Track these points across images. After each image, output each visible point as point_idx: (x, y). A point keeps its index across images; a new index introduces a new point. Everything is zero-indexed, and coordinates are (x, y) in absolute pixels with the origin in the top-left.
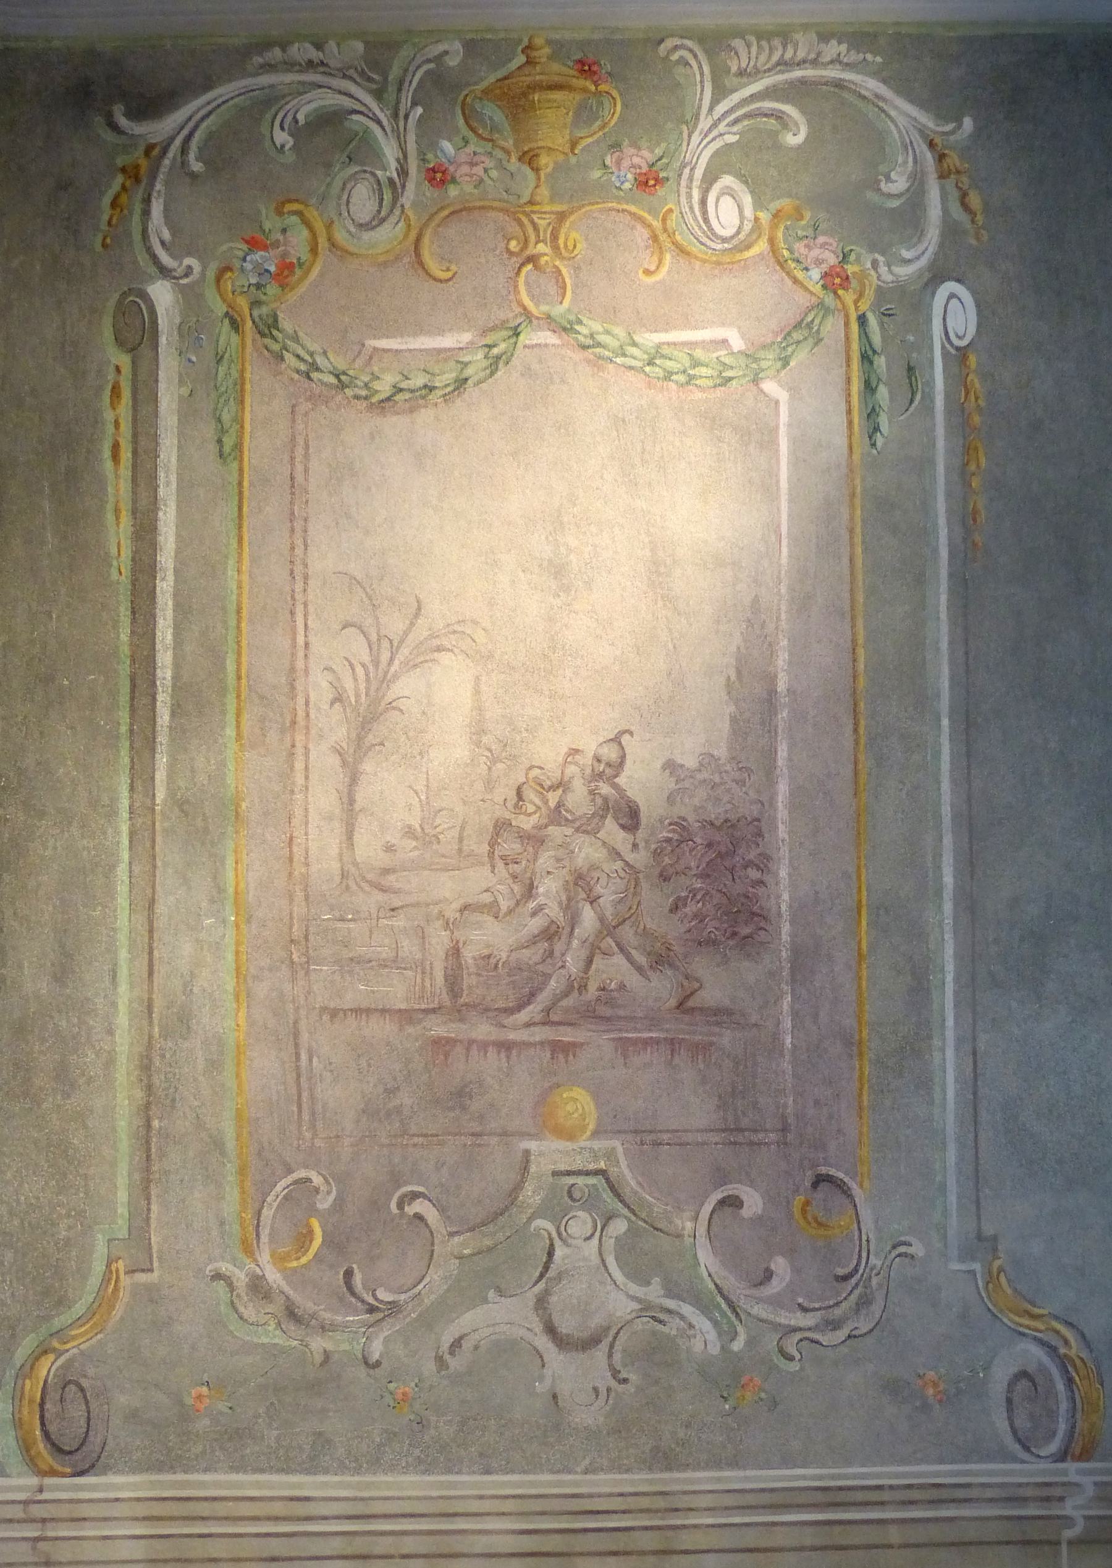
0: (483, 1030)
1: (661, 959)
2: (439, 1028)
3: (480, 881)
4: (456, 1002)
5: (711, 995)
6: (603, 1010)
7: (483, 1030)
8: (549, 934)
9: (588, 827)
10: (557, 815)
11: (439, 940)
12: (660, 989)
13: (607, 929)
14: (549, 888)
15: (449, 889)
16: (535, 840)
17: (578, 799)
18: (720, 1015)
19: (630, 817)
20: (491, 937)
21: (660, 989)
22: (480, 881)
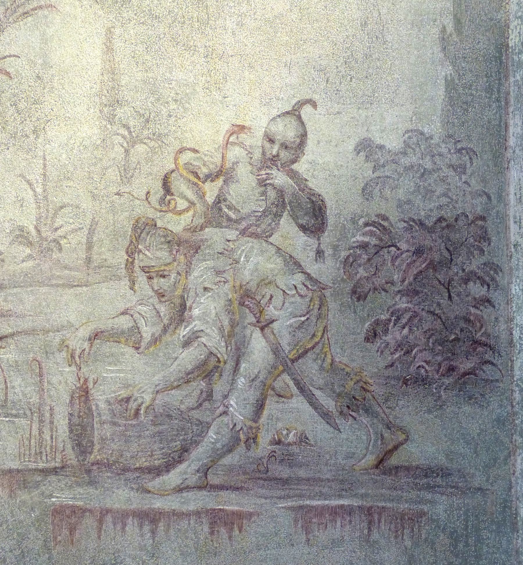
0: (121, 496)
1: (355, 403)
2: (63, 494)
3: (114, 300)
4: (85, 459)
5: (421, 449)
6: (276, 469)
7: (121, 496)
8: (208, 369)
9: (256, 230)
10: (217, 213)
11: (62, 379)
12: (352, 442)
13: (284, 362)
14: (207, 310)
15: (74, 311)
16: (188, 246)
17: (244, 191)
18: (430, 476)
19: (314, 216)
20: (131, 375)
21: (352, 442)
22: (114, 300)
